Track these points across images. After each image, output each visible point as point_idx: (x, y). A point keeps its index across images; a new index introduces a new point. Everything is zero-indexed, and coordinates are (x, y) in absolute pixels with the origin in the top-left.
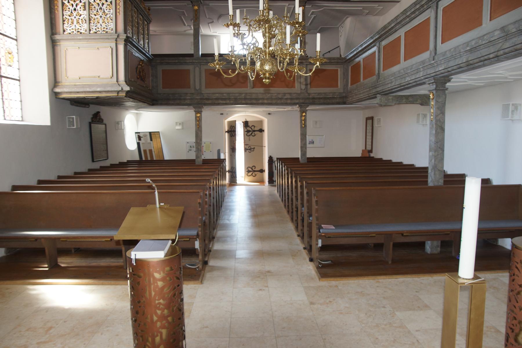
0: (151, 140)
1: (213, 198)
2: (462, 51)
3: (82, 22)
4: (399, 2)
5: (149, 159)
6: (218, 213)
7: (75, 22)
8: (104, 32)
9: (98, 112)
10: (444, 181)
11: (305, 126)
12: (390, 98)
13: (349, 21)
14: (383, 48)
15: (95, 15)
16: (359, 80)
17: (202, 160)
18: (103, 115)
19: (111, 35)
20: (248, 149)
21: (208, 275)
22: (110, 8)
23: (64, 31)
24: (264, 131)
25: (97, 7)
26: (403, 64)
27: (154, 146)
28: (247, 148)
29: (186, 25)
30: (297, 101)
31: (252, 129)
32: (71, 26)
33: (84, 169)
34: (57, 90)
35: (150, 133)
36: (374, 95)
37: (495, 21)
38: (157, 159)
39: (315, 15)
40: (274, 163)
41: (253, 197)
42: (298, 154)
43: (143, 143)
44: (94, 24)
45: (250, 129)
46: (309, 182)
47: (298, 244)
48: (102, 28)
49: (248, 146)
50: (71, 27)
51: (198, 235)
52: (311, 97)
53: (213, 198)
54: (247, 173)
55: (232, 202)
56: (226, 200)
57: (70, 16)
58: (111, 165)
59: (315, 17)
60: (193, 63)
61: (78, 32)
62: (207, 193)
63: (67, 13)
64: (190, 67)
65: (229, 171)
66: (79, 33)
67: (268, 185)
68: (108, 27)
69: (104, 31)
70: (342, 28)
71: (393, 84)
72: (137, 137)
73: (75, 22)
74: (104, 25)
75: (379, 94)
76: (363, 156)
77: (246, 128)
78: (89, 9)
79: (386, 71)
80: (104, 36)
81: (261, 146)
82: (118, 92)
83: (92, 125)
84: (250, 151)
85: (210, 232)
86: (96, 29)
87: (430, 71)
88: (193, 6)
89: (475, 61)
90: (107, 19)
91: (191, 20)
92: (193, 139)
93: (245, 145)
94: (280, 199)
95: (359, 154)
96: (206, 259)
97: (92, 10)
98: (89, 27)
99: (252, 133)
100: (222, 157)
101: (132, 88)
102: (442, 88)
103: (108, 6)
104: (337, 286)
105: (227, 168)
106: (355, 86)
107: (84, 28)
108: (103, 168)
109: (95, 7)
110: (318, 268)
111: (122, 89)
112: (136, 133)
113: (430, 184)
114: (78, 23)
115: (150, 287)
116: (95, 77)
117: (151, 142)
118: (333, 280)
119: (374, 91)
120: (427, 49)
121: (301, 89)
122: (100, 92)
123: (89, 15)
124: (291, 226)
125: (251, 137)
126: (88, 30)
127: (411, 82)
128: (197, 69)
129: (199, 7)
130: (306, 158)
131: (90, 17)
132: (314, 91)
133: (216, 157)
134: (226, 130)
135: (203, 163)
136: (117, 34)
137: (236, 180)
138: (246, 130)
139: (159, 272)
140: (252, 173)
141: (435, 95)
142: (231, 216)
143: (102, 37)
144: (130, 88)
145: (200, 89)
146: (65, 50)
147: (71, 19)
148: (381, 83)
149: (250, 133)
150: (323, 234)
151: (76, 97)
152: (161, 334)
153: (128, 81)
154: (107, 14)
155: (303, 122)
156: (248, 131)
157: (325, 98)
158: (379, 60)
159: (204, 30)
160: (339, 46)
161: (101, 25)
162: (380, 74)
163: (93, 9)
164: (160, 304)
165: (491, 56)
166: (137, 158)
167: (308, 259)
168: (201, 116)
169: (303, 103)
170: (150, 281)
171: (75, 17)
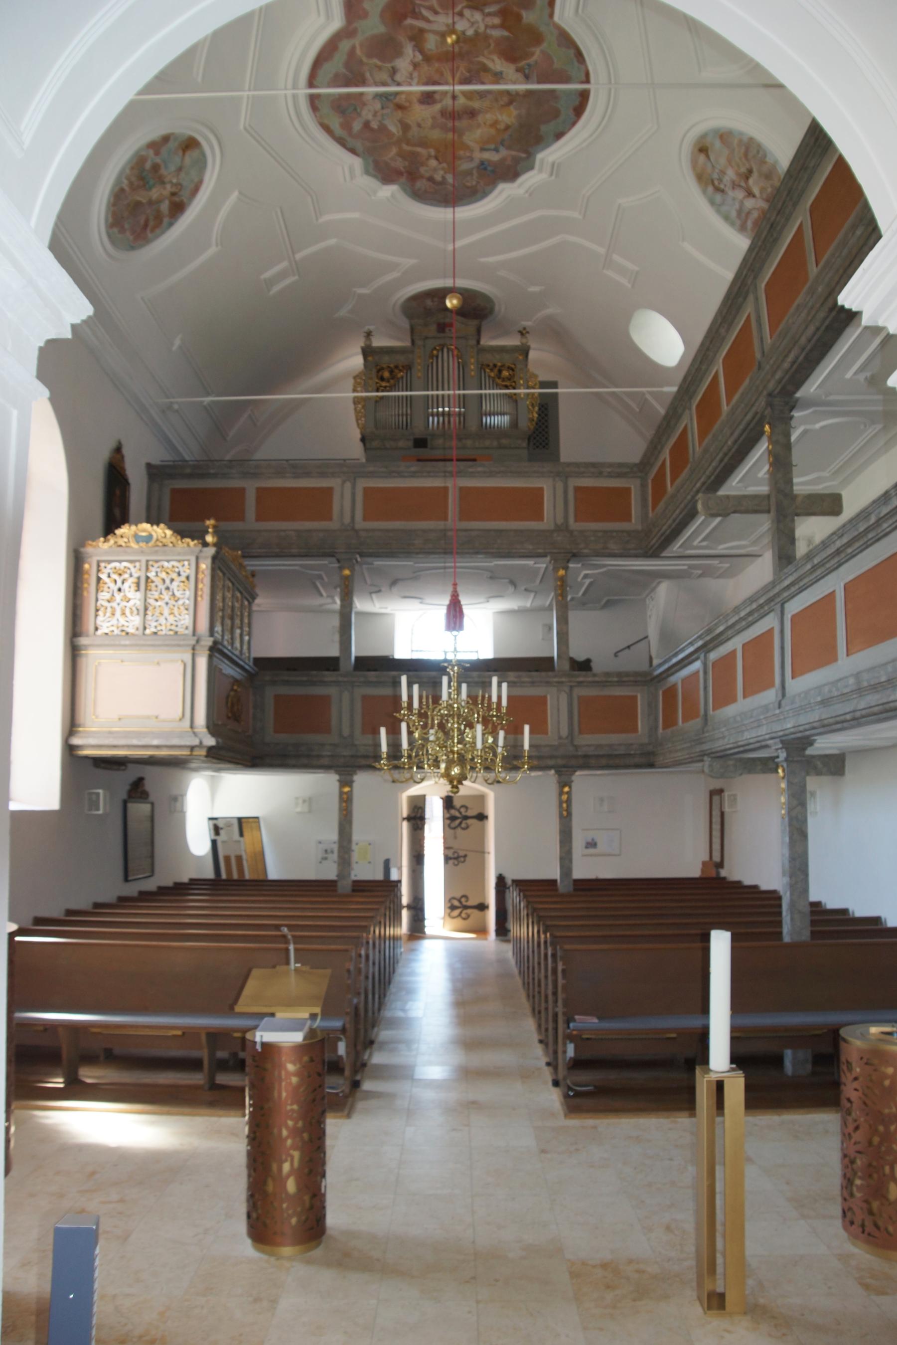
0: (241, 834)
1: (374, 964)
2: (812, 701)
3: (132, 613)
4: (760, 556)
5: (235, 876)
6: (382, 996)
7: (118, 613)
8: (172, 633)
9: (141, 780)
10: (812, 932)
11: (569, 814)
12: (731, 763)
13: (663, 589)
14: (713, 665)
15: (157, 600)
16: (675, 723)
17: (350, 883)
18: (148, 786)
19: (184, 640)
20: (453, 857)
21: (360, 1105)
22: (184, 587)
23: (96, 629)
24: (486, 817)
25: (162, 587)
26: (741, 706)
27: (245, 846)
28: (451, 855)
29: (324, 594)
30: (551, 762)
31: (460, 813)
32: (110, 619)
33: (109, 896)
34: (75, 741)
35: (240, 820)
36: (698, 756)
37: (854, 657)
38: (255, 877)
39: (592, 580)
40: (507, 891)
41: (458, 965)
42: (553, 872)
43: (223, 842)
44: (153, 615)
45: (457, 814)
46: (558, 934)
47: (538, 1056)
48: (168, 624)
49: (452, 851)
50: (109, 622)
51: (344, 1030)
52: (580, 753)
53: (374, 964)
54: (449, 911)
55: (413, 974)
56: (400, 970)
57: (109, 601)
58: (160, 888)
59: (591, 584)
60: (337, 683)
61: (123, 631)
62: (363, 952)
63: (104, 595)
64: (332, 691)
65: (409, 907)
66: (124, 634)
67: (496, 940)
68: (179, 624)
69: (171, 630)
70: (652, 600)
71: (726, 740)
72: (212, 827)
73: (118, 613)
74: (171, 619)
75: (708, 755)
76: (704, 876)
77: (448, 812)
78: (146, 589)
79: (718, 712)
80: (172, 641)
81: (482, 852)
82: (192, 748)
83: (129, 805)
84: (456, 863)
85: (366, 1031)
86: (156, 627)
87: (777, 727)
88: (341, 568)
89: (831, 721)
90: (179, 608)
91: (335, 588)
92: (333, 835)
93: (447, 848)
94: (515, 971)
95: (693, 871)
96: (358, 1078)
97: (150, 590)
98: (144, 623)
99: (460, 823)
100: (394, 876)
101: (220, 740)
102: (799, 759)
103: (182, 584)
104: (595, 1127)
105: (405, 900)
106: (669, 731)
107: (134, 623)
108: (145, 896)
109: (156, 586)
110: (566, 1096)
111: (201, 743)
112: (210, 819)
113: (787, 938)
114: (123, 614)
115: (280, 1085)
116: (148, 717)
117: (241, 839)
118: (591, 1118)
119: (698, 749)
120: (771, 685)
121: (560, 738)
122: (158, 747)
123: (145, 600)
124: (530, 1024)
125: (459, 830)
126: (141, 628)
127: (752, 741)
128: (346, 696)
129: (352, 570)
130: (572, 883)
131: (147, 604)
132: (589, 741)
133: (380, 876)
134: (405, 815)
135: (354, 891)
136: (195, 638)
137: (424, 927)
138: (448, 815)
139: (294, 1063)
140: (461, 913)
141: (786, 771)
142: (410, 1003)
143: (167, 642)
144: (217, 742)
145: (352, 735)
146: (96, 666)
147: (111, 607)
148: (707, 735)
149: (457, 822)
150: (575, 1033)
151: (109, 756)
152: (292, 1158)
153: (213, 727)
154: (179, 599)
155: (565, 805)
156: (452, 818)
157: (609, 756)
158: (705, 688)
159: (361, 604)
160: (646, 637)
161: (166, 619)
162: (709, 716)
163: (154, 588)
164: (292, 1110)
165: (848, 717)
166: (209, 874)
167: (550, 1083)
168: (351, 791)
169: (564, 766)
170: (280, 1074)
171: (119, 604)
